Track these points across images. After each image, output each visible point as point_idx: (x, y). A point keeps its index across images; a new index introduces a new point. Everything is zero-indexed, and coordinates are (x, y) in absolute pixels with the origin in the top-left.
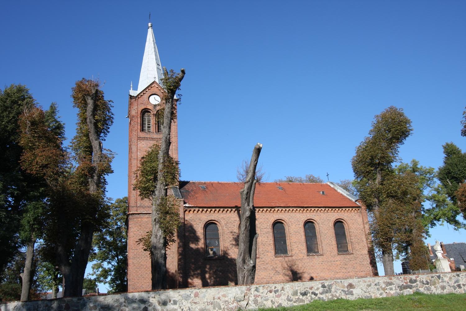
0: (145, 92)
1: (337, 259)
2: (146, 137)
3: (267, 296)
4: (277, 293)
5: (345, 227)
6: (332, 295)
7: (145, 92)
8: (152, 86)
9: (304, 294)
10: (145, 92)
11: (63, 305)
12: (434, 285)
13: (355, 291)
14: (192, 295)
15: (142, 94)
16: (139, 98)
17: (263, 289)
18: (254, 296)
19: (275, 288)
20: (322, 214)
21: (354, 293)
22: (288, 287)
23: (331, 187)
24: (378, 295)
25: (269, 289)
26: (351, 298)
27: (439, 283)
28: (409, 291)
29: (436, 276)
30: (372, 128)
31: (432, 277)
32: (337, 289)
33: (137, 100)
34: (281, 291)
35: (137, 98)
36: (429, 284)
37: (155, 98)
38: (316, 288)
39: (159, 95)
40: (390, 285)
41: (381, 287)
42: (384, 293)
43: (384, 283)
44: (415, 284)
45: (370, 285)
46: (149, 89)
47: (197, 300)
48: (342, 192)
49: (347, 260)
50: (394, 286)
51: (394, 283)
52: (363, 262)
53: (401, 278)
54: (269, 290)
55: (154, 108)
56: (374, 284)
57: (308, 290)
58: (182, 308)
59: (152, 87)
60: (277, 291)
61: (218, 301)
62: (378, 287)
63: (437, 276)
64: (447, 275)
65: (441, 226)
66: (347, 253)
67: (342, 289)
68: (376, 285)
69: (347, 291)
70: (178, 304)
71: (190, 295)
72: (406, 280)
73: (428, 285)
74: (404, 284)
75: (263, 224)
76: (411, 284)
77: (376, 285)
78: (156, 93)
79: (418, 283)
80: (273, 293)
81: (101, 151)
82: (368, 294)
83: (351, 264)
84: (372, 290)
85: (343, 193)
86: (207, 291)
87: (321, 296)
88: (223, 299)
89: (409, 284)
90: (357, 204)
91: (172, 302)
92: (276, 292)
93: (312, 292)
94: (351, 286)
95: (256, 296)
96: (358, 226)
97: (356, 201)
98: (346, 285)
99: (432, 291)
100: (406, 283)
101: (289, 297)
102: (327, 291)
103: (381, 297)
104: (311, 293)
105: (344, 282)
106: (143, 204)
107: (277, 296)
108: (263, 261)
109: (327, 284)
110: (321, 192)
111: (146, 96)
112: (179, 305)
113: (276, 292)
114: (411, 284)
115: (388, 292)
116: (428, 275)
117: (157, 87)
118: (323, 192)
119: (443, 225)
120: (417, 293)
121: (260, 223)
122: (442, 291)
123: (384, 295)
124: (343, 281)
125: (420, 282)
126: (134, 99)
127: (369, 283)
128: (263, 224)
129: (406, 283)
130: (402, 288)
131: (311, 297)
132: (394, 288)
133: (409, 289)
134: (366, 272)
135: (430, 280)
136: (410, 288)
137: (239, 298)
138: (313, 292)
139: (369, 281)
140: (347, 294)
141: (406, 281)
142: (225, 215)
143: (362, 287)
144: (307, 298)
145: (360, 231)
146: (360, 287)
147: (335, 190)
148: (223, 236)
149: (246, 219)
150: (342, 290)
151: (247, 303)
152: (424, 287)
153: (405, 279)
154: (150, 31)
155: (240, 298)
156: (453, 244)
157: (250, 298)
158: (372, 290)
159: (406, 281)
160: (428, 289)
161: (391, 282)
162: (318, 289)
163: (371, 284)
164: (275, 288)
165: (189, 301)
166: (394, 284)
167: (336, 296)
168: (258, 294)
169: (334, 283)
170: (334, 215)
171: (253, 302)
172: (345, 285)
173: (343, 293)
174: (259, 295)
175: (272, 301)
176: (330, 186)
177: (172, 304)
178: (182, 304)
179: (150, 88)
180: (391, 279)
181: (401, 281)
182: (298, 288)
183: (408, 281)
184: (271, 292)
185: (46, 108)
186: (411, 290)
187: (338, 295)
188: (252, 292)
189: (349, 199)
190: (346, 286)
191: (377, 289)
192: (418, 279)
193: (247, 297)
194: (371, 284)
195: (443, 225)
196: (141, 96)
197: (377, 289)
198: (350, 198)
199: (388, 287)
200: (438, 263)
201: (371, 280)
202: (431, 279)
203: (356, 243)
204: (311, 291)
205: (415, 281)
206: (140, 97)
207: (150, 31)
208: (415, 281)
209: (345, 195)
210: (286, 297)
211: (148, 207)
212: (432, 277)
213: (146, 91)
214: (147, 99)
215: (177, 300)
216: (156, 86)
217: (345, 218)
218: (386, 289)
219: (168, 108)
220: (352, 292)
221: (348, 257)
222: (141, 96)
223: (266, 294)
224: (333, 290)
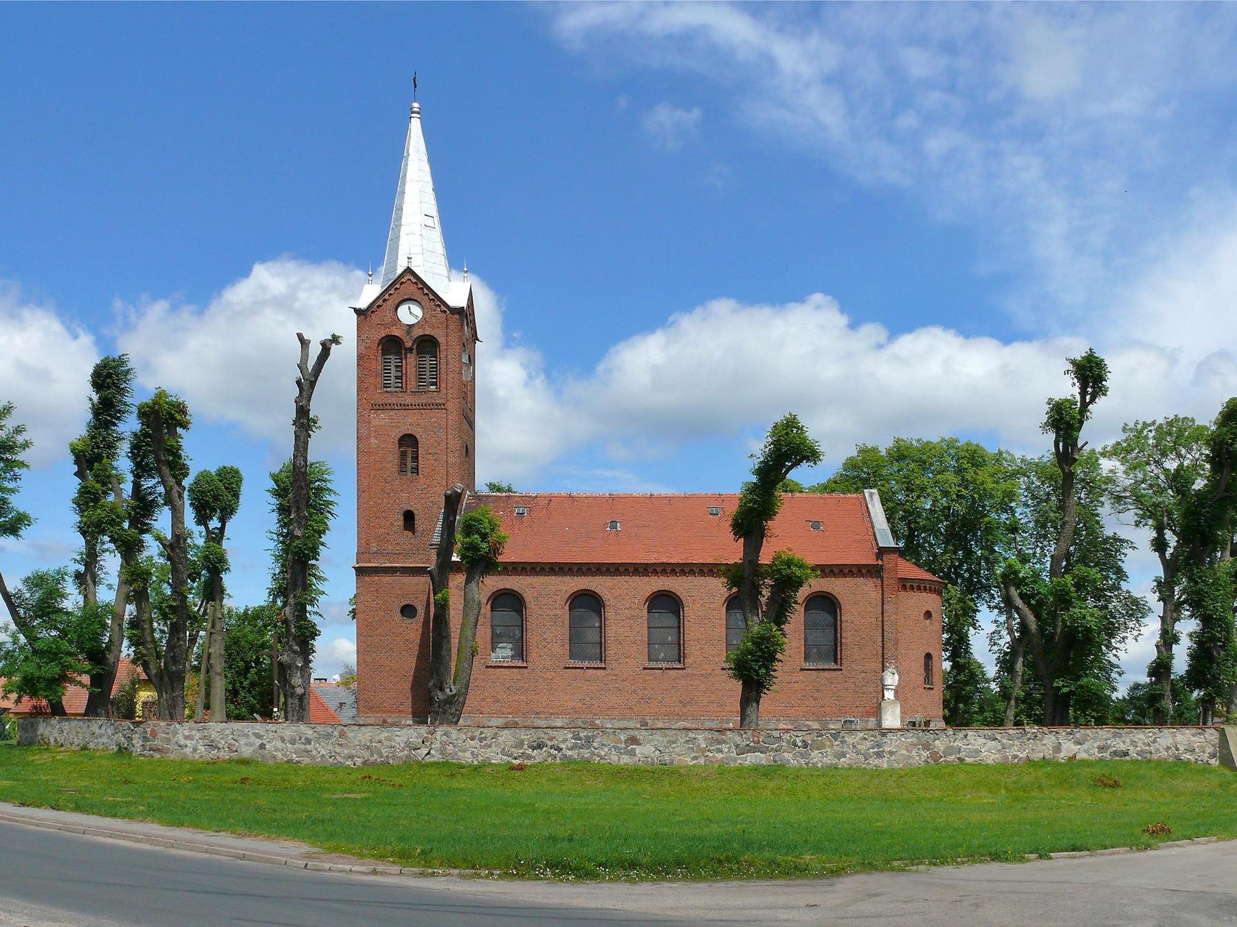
0: (387, 297)
2: (390, 401)
3: (466, 745)
7: (387, 295)
8: (403, 280)
9: (540, 746)
10: (387, 295)
14: (336, 733)
15: (380, 302)
18: (441, 743)
21: (637, 752)
24: (688, 759)
25: (469, 734)
36: (809, 748)
37: (409, 308)
46: (396, 289)
47: (343, 741)
50: (728, 746)
52: (865, 688)
59: (403, 283)
60: (485, 738)
61: (379, 745)
64: (858, 733)
71: (333, 732)
75: (623, 599)
87: (569, 753)
88: (387, 743)
91: (303, 740)
92: (481, 740)
94: (634, 741)
106: (382, 548)
108: (616, 675)
109: (585, 734)
113: (481, 740)
122: (836, 761)
125: (788, 742)
128: (623, 599)
144: (541, 754)
151: (427, 752)
154: (415, 125)
162: (565, 741)
163: (677, 740)
165: (330, 741)
172: (622, 738)
175: (472, 753)
179: (398, 286)
184: (472, 739)
185: (21, 533)
188: (438, 737)
190: (623, 740)
196: (379, 306)
203: (854, 646)
204: (549, 743)
207: (415, 125)
211: (394, 554)
213: (396, 289)
222: (379, 306)
223: (464, 742)
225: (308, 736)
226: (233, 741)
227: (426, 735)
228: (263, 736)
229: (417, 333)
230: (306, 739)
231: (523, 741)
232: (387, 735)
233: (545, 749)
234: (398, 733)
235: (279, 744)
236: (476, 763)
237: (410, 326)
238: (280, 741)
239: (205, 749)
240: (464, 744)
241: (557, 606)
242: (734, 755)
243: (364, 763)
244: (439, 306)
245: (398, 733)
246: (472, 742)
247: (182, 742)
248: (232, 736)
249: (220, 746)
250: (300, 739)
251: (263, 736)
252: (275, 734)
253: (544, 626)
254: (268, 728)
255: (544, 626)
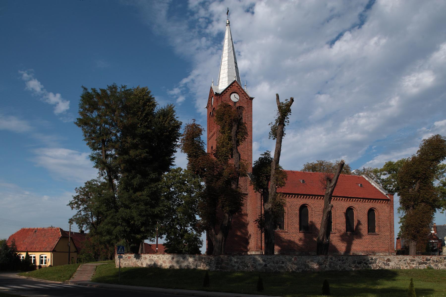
1: (367, 238)
3: (337, 263)
4: (343, 262)
5: (375, 214)
6: (376, 265)
8: (233, 85)
11: (219, 259)
12: (440, 263)
13: (391, 264)
15: (225, 92)
16: (222, 95)
17: (335, 259)
18: (329, 262)
19: (342, 259)
20: (360, 203)
21: (390, 264)
22: (350, 258)
23: (366, 179)
24: (405, 267)
26: (387, 267)
27: (444, 262)
28: (424, 266)
29: (443, 257)
30: (419, 149)
31: (441, 258)
32: (380, 262)
33: (221, 97)
34: (346, 260)
35: (221, 96)
37: (235, 96)
38: (367, 260)
39: (238, 93)
40: (413, 262)
41: (407, 262)
42: (409, 266)
43: (410, 259)
44: (429, 261)
45: (400, 261)
46: (230, 88)
48: (376, 185)
49: (374, 239)
50: (416, 262)
51: (416, 260)
53: (421, 257)
54: (338, 259)
55: (234, 105)
56: (403, 260)
57: (362, 261)
58: (287, 266)
59: (233, 86)
62: (405, 262)
63: (444, 258)
65: (441, 214)
66: (375, 234)
67: (383, 262)
68: (404, 260)
69: (386, 263)
70: (284, 263)
71: (292, 259)
72: (424, 259)
73: (437, 263)
74: (422, 261)
75: (317, 208)
76: (427, 262)
77: (404, 260)
78: (236, 92)
79: (431, 261)
80: (341, 261)
81: (240, 160)
82: (398, 266)
83: (376, 242)
84: (402, 263)
85: (376, 187)
86: (301, 257)
89: (425, 261)
90: (387, 197)
91: (281, 262)
92: (342, 260)
93: (364, 262)
94: (389, 260)
95: (330, 262)
96: (386, 214)
97: (386, 195)
98: (386, 259)
99: (439, 266)
100: (424, 261)
101: (350, 265)
102: (374, 262)
103: (406, 268)
104: (363, 263)
105: (385, 257)
107: (343, 263)
109: (374, 258)
110: (360, 185)
111: (228, 94)
112: (285, 264)
113: (342, 260)
114: (427, 262)
115: (411, 265)
116: (438, 257)
117: (237, 85)
118: (361, 185)
119: (443, 213)
120: (430, 268)
121: (315, 207)
123: (409, 268)
124: (384, 257)
125: (432, 260)
126: (219, 96)
127: (400, 259)
128: (317, 208)
129: (424, 261)
130: (420, 263)
131: (363, 265)
132: (415, 264)
133: (424, 265)
134: (386, 248)
135: (439, 260)
136: (426, 264)
137: (320, 263)
138: (365, 262)
139: (401, 258)
140: (385, 265)
141: (423, 260)
142: (290, 200)
143: (395, 261)
145: (386, 218)
146: (394, 261)
147: (369, 182)
148: (287, 215)
149: (328, 212)
150: (383, 262)
152: (434, 264)
153: (423, 258)
155: (321, 262)
156: (444, 226)
157: (327, 263)
158: (402, 263)
159: (423, 260)
160: (436, 265)
161: (414, 259)
163: (401, 260)
164: (342, 259)
166: (415, 261)
167: (379, 266)
168: (332, 261)
169: (378, 258)
170: (368, 205)
171: (328, 266)
172: (385, 259)
173: (383, 265)
174: (333, 262)
175: (340, 266)
176: (365, 179)
177: (281, 263)
178: (287, 264)
179: (231, 87)
180: (414, 258)
181: (421, 259)
182: (356, 259)
183: (425, 260)
184: (340, 260)
186: (426, 265)
187: (380, 265)
189: (381, 192)
190: (386, 260)
191: (405, 263)
192: (431, 258)
193: (325, 262)
194: (401, 260)
195: (443, 213)
196: (224, 93)
197: (405, 263)
198: (382, 191)
199: (412, 263)
200: (445, 249)
201: (402, 257)
202: (439, 259)
204: (364, 262)
205: (429, 260)
206: (223, 94)
208: (429, 260)
209: (378, 188)
210: (348, 264)
212: (441, 258)
213: (228, 89)
214: (229, 97)
215: (284, 261)
216: (236, 85)
217: (377, 207)
218: (411, 264)
219: (281, 128)
220: (389, 264)
221: (375, 237)
223: (337, 262)
224: (377, 262)
225: (283, 260)
226: (253, 263)
227: (325, 259)
228: (266, 261)
229: (237, 105)
230: (282, 262)
231: (355, 261)
232: (311, 259)
233: (362, 264)
234: (315, 259)
235: (272, 264)
236: (341, 270)
237: (235, 103)
238: (272, 263)
239: (242, 267)
240: (337, 262)
241: (297, 210)
242: (418, 265)
243: (302, 271)
244: (245, 96)
245: (315, 259)
246: (340, 262)
247: (234, 264)
248: (253, 261)
249: (249, 265)
250: (280, 262)
251: (266, 261)
252: (271, 260)
253: (293, 217)
254: (268, 257)
255: (293, 217)
